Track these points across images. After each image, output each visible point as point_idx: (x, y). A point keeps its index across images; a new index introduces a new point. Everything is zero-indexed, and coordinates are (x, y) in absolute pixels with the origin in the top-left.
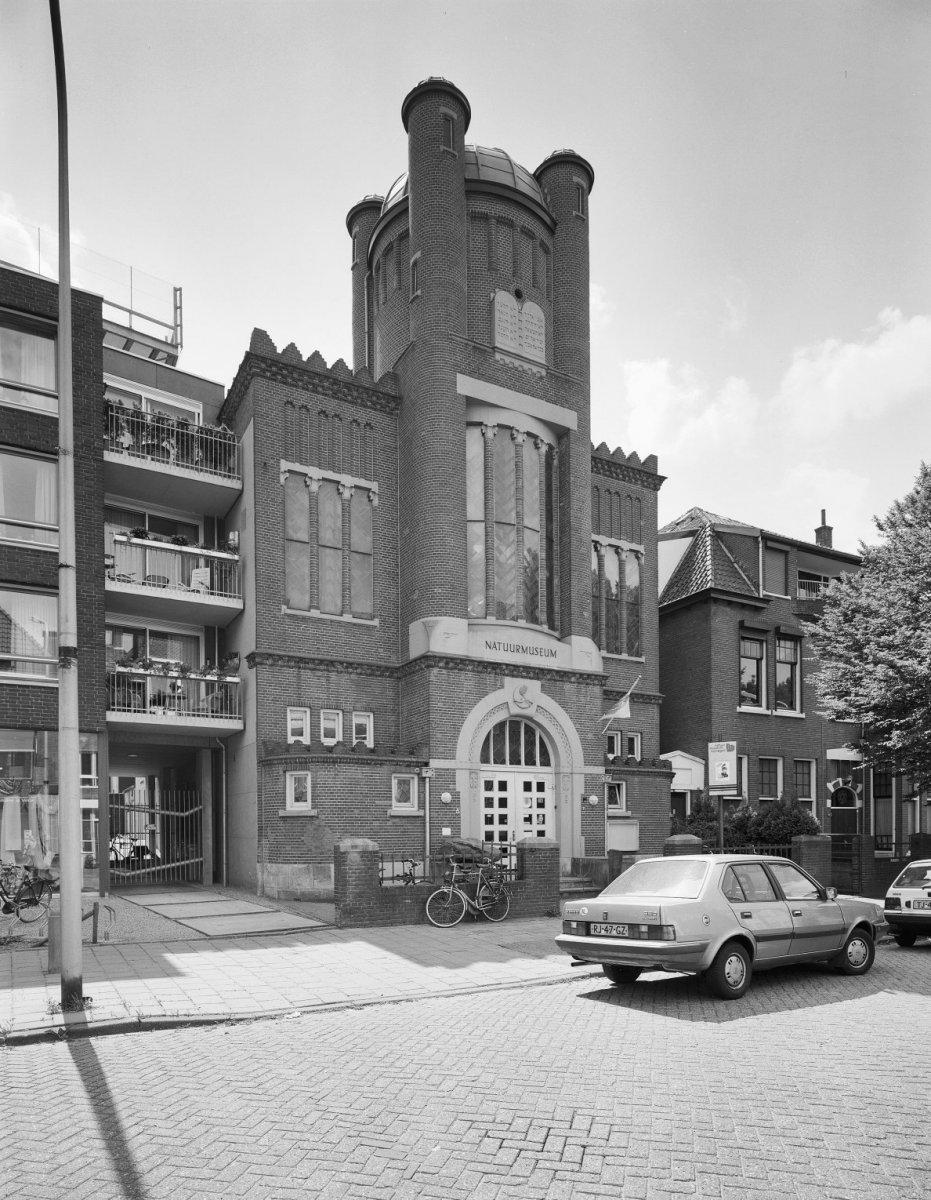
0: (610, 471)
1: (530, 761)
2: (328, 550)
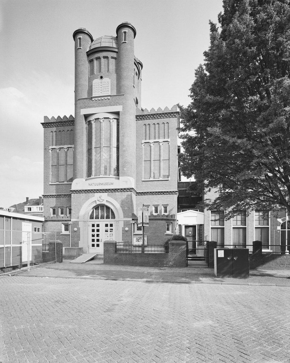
0: (154, 117)
1: (108, 217)
2: (61, 166)
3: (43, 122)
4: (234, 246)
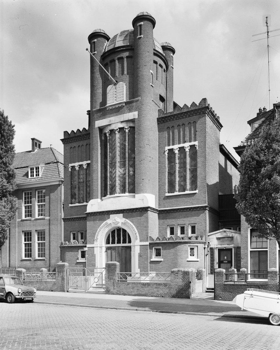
3: (63, 138)
4: (254, 271)
